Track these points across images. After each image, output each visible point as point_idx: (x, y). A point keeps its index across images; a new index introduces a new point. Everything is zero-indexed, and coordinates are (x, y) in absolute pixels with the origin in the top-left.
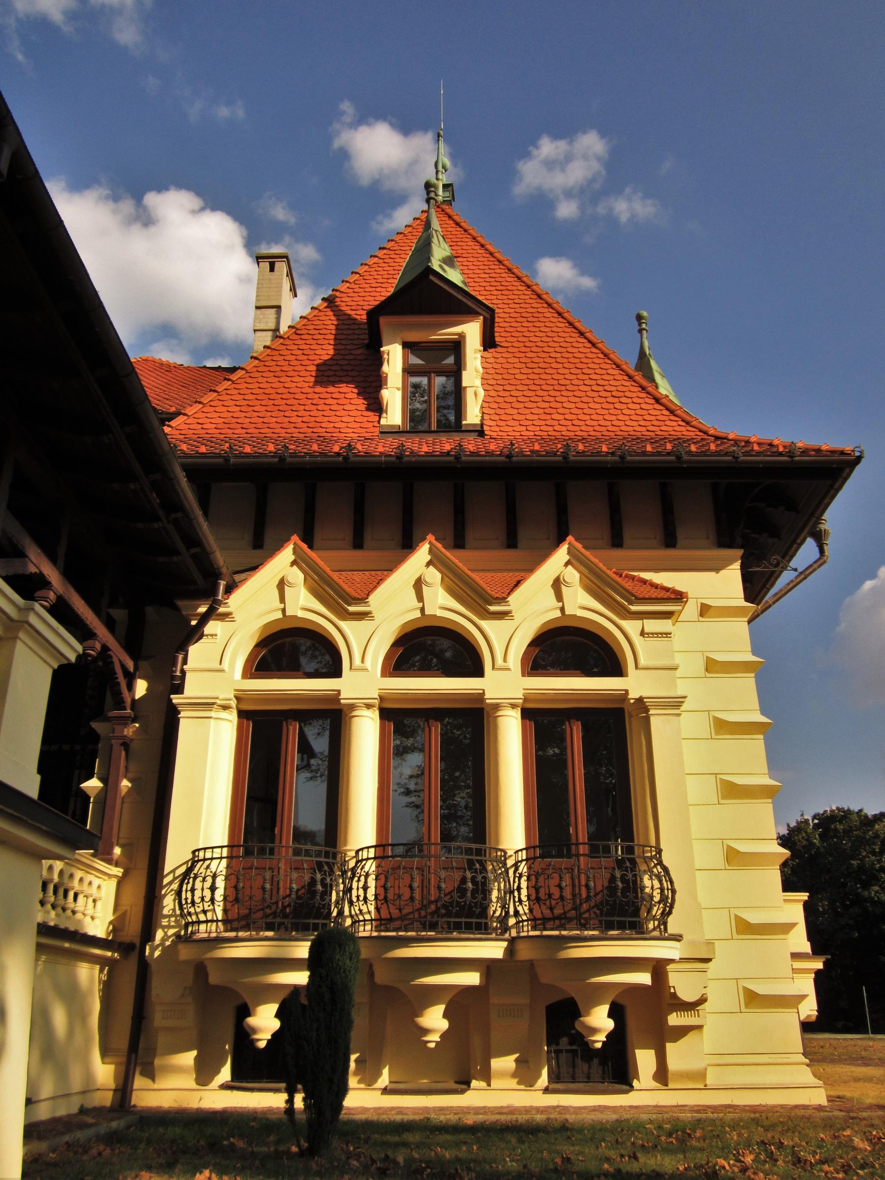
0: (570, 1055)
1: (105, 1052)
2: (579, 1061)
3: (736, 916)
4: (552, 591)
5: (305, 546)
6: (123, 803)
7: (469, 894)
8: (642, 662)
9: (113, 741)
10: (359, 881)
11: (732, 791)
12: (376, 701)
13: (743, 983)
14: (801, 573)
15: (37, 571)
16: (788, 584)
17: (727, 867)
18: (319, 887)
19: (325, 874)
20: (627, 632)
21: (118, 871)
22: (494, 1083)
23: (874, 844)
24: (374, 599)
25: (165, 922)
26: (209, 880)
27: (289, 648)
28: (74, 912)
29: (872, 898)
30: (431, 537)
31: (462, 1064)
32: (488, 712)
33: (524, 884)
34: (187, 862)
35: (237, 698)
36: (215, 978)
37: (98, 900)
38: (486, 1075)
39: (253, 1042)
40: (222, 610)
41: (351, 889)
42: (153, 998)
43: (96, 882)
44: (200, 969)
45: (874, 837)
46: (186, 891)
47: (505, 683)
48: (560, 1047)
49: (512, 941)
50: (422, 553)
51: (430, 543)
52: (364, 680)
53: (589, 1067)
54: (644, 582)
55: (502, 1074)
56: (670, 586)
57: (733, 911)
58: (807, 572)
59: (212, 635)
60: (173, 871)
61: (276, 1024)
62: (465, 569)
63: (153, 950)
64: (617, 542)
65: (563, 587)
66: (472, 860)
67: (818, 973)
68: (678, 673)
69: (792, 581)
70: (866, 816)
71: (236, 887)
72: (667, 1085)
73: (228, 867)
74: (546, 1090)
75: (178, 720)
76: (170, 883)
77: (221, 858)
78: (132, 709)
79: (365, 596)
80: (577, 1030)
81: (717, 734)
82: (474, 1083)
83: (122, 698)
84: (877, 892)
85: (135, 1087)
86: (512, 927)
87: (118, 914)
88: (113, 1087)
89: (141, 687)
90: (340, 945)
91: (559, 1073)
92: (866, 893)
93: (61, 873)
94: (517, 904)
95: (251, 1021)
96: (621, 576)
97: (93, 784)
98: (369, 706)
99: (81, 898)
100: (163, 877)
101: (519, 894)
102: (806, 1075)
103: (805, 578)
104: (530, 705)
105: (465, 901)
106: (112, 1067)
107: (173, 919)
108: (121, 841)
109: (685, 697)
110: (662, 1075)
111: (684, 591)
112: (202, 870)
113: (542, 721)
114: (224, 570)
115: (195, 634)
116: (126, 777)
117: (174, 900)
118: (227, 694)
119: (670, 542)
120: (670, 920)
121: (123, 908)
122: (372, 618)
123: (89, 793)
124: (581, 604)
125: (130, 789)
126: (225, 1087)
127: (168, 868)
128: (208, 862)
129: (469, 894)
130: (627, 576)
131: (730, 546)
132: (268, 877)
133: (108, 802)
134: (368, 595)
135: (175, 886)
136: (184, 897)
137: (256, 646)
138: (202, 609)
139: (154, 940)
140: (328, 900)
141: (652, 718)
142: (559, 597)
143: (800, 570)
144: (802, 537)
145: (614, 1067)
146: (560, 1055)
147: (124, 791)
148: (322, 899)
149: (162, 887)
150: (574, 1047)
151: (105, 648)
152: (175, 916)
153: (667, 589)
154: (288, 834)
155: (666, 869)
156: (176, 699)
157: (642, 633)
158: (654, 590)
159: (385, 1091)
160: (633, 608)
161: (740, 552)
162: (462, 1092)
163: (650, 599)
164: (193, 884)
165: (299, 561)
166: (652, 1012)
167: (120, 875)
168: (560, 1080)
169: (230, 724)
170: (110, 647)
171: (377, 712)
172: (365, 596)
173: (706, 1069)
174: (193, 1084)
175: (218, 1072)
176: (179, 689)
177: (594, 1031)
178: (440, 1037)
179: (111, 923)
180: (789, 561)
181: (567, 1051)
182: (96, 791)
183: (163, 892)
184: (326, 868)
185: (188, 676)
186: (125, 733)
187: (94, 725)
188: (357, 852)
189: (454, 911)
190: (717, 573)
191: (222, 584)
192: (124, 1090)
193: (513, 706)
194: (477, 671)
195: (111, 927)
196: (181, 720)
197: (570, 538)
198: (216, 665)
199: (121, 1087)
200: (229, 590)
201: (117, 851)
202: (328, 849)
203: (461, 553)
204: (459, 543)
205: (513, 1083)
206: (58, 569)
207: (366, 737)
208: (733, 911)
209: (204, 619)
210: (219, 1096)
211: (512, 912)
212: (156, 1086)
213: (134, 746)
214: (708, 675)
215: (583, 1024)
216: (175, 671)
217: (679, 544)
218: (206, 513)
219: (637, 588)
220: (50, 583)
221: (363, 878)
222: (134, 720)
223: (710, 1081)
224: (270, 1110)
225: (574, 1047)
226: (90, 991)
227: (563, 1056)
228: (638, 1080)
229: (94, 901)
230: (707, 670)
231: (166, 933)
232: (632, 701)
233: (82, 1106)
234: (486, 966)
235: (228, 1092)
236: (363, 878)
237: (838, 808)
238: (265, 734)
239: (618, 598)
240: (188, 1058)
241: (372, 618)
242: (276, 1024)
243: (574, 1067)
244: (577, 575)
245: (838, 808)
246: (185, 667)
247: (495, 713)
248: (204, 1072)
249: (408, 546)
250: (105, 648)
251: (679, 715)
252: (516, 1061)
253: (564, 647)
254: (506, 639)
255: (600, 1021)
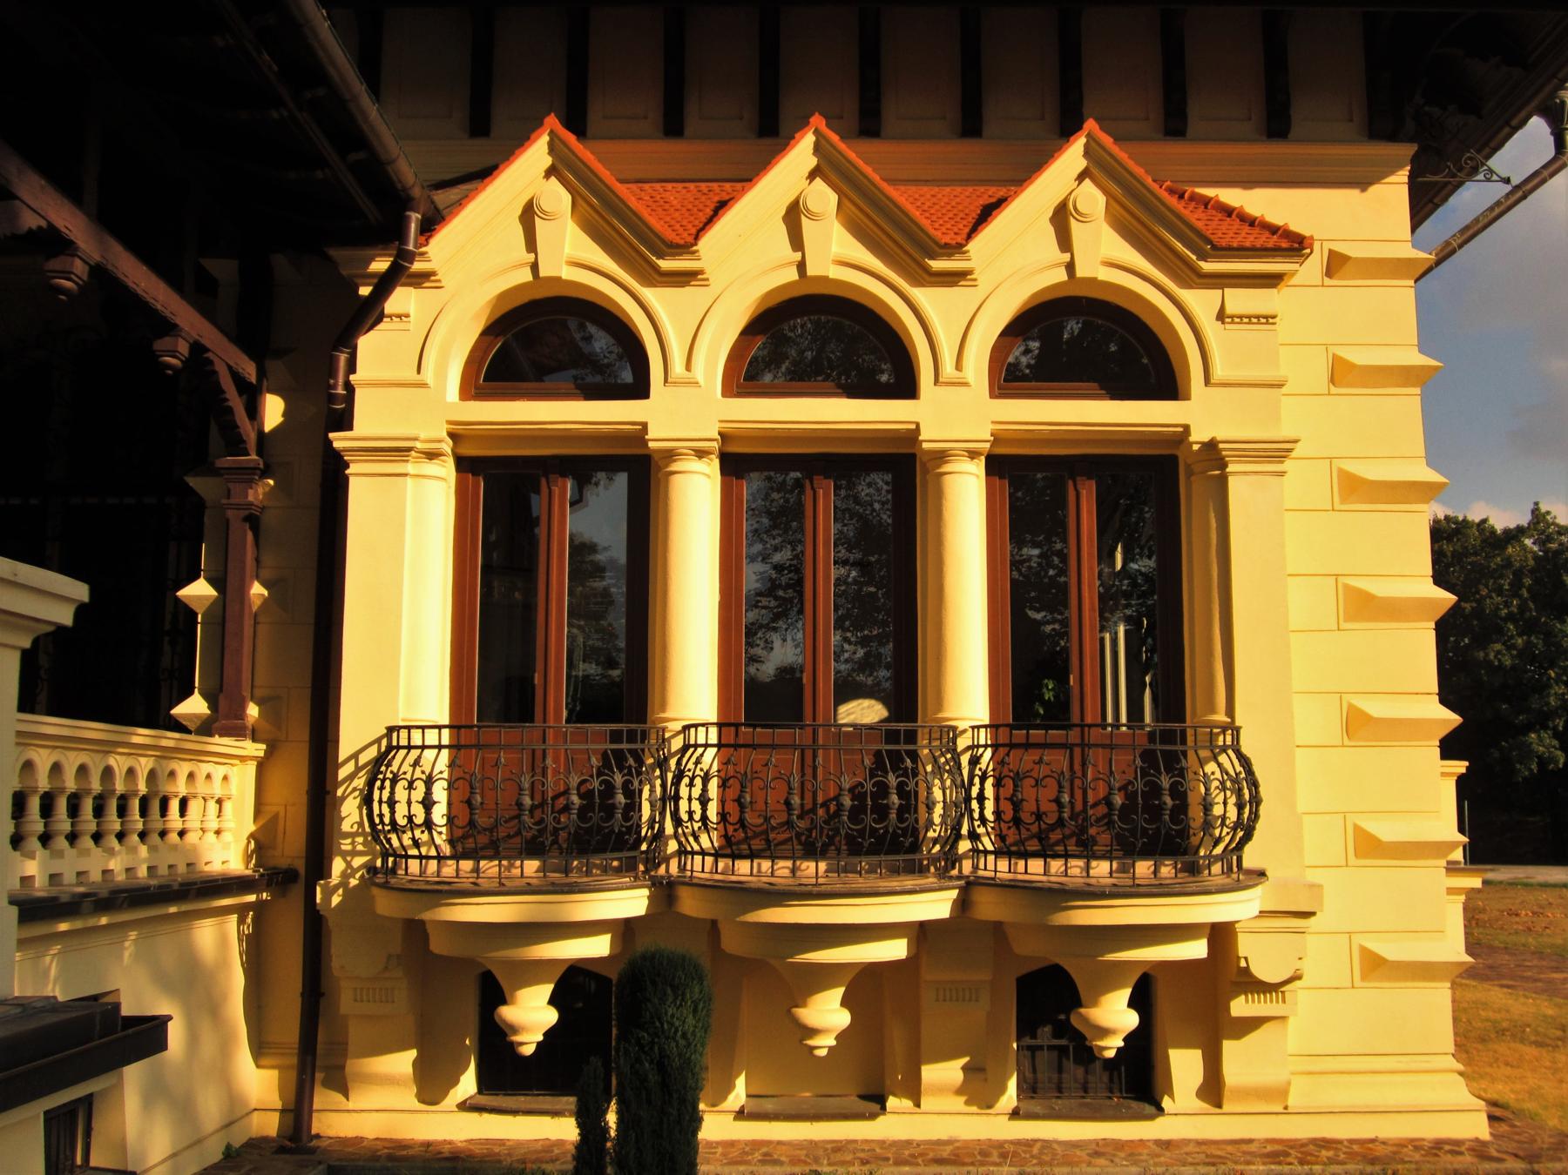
0: (1055, 1054)
1: (260, 1050)
2: (1069, 1065)
3: (1357, 828)
4: (1051, 231)
5: (571, 138)
6: (256, 623)
7: (893, 816)
8: (1218, 372)
9: (230, 513)
10: (691, 785)
11: (1363, 607)
12: (715, 444)
13: (1359, 940)
14: (1517, 188)
15: (43, 224)
16: (1491, 209)
17: (1347, 742)
18: (621, 799)
19: (630, 773)
20: (1192, 313)
21: (257, 749)
22: (926, 1102)
23: (1502, 576)
24: (708, 244)
25: (346, 845)
26: (420, 788)
27: (544, 340)
28: (182, 834)
29: (1490, 663)
30: (817, 120)
31: (873, 1075)
32: (924, 465)
33: (989, 792)
34: (378, 741)
35: (452, 435)
36: (438, 945)
37: (222, 806)
38: (913, 1091)
39: (512, 1047)
40: (417, 266)
41: (677, 798)
42: (336, 973)
43: (219, 772)
44: (416, 931)
45: (1503, 567)
46: (380, 802)
47: (958, 411)
48: (1039, 1042)
49: (969, 887)
50: (801, 154)
51: (816, 132)
52: (690, 405)
53: (1087, 1072)
54: (1228, 211)
55: (940, 1090)
56: (1280, 223)
57: (1351, 819)
58: (1529, 186)
59: (399, 316)
60: (355, 756)
61: (551, 1016)
62: (876, 178)
63: (329, 893)
64: (1175, 125)
65: (1073, 223)
66: (898, 752)
67: (1471, 893)
68: (1284, 390)
69: (1498, 203)
70: (1493, 531)
71: (469, 802)
72: (1220, 1106)
73: (451, 765)
74: (1015, 1114)
75: (346, 479)
76: (351, 777)
77: (440, 747)
78: (259, 454)
79: (690, 239)
80: (1068, 1019)
81: (1343, 501)
82: (892, 1102)
83: (240, 435)
84: (1499, 652)
85: (315, 1107)
86: (965, 856)
87: (261, 822)
88: (279, 1105)
89: (273, 410)
90: (675, 988)
91: (1036, 1081)
92: (1482, 654)
93: (152, 775)
94: (977, 823)
95: (508, 1013)
96: (1181, 197)
97: (199, 590)
98: (701, 454)
99: (194, 807)
100: (338, 766)
101: (982, 808)
102: (1458, 1092)
103: (1524, 197)
104: (1002, 450)
105: (886, 828)
106: (274, 1074)
107: (360, 839)
108: (258, 693)
109: (1296, 442)
110: (1213, 1090)
111: (1307, 233)
112: (406, 767)
113: (1024, 478)
114: (416, 192)
115: (368, 313)
116: (258, 578)
117: (360, 808)
118: (434, 431)
119: (1277, 126)
120: (1248, 849)
121: (269, 810)
122: (705, 283)
123: (194, 606)
124: (1107, 257)
125: (266, 601)
126: (465, 1106)
127: (344, 751)
128: (414, 753)
129: (893, 816)
130: (1194, 198)
131: (1392, 137)
132: (527, 785)
133: (230, 626)
134: (697, 238)
135: (360, 782)
136: (376, 811)
137: (484, 333)
138: (380, 265)
139: (330, 876)
140: (636, 817)
141: (1232, 481)
142: (1065, 242)
143: (1515, 181)
144: (1523, 114)
145: (1136, 1079)
146: (1038, 1054)
147: (256, 604)
148: (626, 818)
149: (337, 785)
150: (1064, 1042)
151: (198, 349)
152: (364, 834)
153: (1273, 229)
154: (559, 652)
155: (1245, 761)
156: (339, 440)
157: (1221, 316)
158: (1246, 229)
159: (741, 1114)
160: (1208, 266)
161: (1410, 150)
162: (873, 1116)
163: (1241, 249)
164: (392, 792)
165: (560, 166)
166: (1205, 999)
167: (262, 754)
168: (1041, 1095)
169: (442, 484)
170: (208, 344)
171: (716, 462)
172: (690, 239)
173: (1289, 1083)
174: (415, 1104)
175: (455, 1082)
176: (344, 421)
177: (1105, 1032)
178: (837, 1038)
179: (252, 836)
180: (1488, 157)
181: (1051, 1048)
182: (208, 604)
183: (339, 792)
184: (631, 761)
185: (360, 395)
186: (251, 498)
187: (192, 481)
188: (686, 728)
189: (866, 844)
190: (1364, 190)
191: (415, 218)
192: (297, 1111)
193: (973, 454)
194: (905, 387)
195: (252, 845)
196: (352, 480)
197: (1090, 125)
198: (410, 374)
199: (292, 1107)
200: (429, 226)
201: (253, 711)
202: (633, 726)
203: (872, 146)
204: (868, 125)
205: (959, 1103)
206: (88, 215)
207: (696, 509)
208: (1351, 819)
209: (385, 284)
210: (456, 1121)
211: (964, 831)
212: (351, 1105)
213: (268, 520)
214: (1334, 390)
215: (1086, 1020)
216: (335, 387)
217: (1295, 130)
218: (375, 90)
219: (1214, 224)
220: (72, 242)
221: (698, 781)
222: (265, 473)
223: (1293, 1101)
224: (550, 1146)
225: (1064, 1042)
226: (224, 963)
227: (1044, 1057)
228: (1172, 1096)
229: (219, 802)
230: (1332, 380)
231: (349, 864)
232: (1196, 447)
233: (228, 1147)
234: (921, 932)
235: (475, 1116)
236: (698, 781)
237: (1447, 518)
238: (505, 497)
239: (1179, 246)
240: (403, 1062)
241: (705, 283)
242: (551, 1016)
243: (1060, 1070)
244: (1101, 199)
245: (1447, 518)
246: (352, 377)
247: (939, 466)
248: (431, 1083)
249: (772, 134)
250: (198, 349)
251: (1282, 474)
252: (965, 1068)
253: (1075, 339)
254: (958, 322)
255: (1115, 1016)
